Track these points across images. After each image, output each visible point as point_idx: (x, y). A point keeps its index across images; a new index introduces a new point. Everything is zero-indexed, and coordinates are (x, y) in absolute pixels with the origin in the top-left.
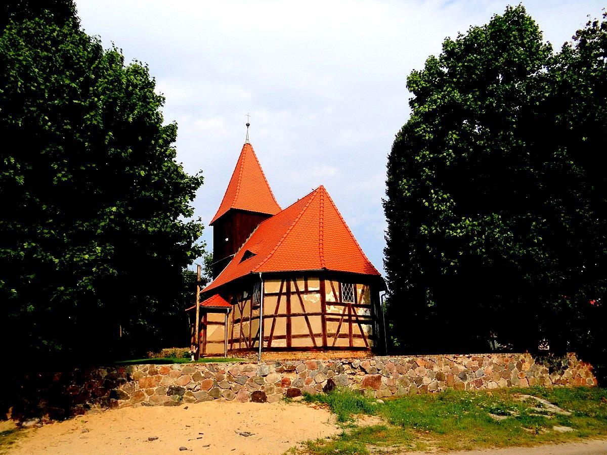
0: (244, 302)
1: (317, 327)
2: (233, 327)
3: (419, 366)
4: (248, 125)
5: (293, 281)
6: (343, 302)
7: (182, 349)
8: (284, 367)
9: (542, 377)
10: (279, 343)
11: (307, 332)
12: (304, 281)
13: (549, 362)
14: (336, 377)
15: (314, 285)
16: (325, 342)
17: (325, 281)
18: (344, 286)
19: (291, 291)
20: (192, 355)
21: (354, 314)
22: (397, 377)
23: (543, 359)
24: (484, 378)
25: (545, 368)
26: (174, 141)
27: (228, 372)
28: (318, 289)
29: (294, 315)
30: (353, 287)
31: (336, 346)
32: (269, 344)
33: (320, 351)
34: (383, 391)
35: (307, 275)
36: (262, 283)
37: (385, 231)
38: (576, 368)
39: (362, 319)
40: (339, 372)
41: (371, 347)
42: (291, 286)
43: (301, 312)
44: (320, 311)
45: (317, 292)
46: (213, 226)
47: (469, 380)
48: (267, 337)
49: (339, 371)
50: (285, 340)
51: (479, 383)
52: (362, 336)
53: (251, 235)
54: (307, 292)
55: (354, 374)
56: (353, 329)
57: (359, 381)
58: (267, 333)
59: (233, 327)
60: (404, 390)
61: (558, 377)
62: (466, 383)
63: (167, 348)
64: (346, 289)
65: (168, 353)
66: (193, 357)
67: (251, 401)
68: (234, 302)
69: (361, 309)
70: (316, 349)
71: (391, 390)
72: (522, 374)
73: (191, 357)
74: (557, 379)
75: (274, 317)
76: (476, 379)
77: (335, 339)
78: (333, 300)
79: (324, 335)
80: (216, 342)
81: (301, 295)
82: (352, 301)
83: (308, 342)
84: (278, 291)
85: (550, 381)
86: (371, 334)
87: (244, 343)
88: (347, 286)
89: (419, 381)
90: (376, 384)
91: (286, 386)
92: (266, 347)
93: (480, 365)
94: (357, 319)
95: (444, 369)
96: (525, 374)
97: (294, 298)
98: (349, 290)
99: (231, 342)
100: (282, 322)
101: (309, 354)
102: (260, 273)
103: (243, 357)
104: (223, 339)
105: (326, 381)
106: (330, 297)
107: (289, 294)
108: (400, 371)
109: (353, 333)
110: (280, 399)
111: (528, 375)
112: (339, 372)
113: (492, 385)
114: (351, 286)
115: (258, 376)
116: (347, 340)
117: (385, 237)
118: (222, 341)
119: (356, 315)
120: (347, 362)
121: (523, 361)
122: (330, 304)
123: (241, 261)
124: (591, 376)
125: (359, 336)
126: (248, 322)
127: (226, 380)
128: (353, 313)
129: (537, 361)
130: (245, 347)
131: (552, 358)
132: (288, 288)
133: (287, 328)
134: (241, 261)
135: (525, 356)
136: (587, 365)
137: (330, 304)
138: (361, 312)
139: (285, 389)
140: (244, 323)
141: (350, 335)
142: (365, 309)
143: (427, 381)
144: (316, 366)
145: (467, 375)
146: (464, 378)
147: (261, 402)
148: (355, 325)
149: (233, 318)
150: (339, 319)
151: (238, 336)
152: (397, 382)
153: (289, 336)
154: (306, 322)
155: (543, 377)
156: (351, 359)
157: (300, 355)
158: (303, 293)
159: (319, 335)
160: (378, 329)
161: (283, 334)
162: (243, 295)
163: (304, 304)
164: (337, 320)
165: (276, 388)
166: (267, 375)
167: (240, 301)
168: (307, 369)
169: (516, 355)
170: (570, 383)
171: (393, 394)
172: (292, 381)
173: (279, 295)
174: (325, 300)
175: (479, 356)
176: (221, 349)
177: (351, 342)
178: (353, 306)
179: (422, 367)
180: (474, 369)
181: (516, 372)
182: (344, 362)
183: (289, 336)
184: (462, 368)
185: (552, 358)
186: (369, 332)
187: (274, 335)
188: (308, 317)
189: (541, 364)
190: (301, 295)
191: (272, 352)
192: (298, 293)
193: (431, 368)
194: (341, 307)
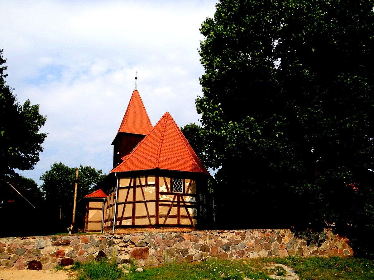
1: (152, 212)
3: (185, 240)
4: (136, 78)
6: (173, 192)
8: (60, 241)
9: (300, 249)
10: (127, 222)
11: (145, 214)
12: (155, 177)
13: (307, 235)
14: (107, 249)
15: (152, 180)
16: (157, 221)
17: (160, 177)
19: (137, 185)
20: (70, 231)
21: (182, 201)
22: (163, 249)
23: (301, 234)
24: (246, 250)
25: (303, 241)
26: (3, 67)
27: (9, 245)
28: (154, 183)
29: (138, 202)
30: (182, 181)
31: (166, 224)
32: (121, 223)
34: (151, 260)
35: (147, 173)
36: (118, 180)
38: (333, 241)
40: (110, 245)
43: (142, 199)
44: (154, 198)
45: (153, 185)
47: (232, 251)
48: (119, 218)
49: (110, 244)
50: (131, 220)
51: (241, 253)
52: (188, 217)
54: (147, 185)
55: (126, 247)
57: (129, 252)
58: (120, 215)
60: (169, 260)
61: (315, 248)
62: (229, 253)
64: (176, 183)
66: (70, 232)
67: (27, 269)
69: (188, 197)
70: (151, 226)
71: (158, 260)
72: (282, 246)
73: (69, 233)
74: (314, 250)
76: (238, 250)
78: (165, 191)
79: (157, 216)
80: (95, 222)
81: (143, 188)
82: (181, 192)
83: (145, 222)
84: (128, 186)
85: (308, 252)
86: (196, 215)
88: (178, 180)
89: (185, 252)
90: (144, 254)
91: (60, 256)
92: (118, 225)
93: (243, 239)
94: (185, 204)
95: (208, 242)
96: (285, 246)
97: (138, 190)
98: (179, 183)
100: (129, 207)
101: (147, 230)
102: (116, 173)
105: (98, 253)
106: (163, 189)
107: (135, 187)
108: (168, 244)
109: (181, 215)
110: (54, 268)
111: (287, 246)
112: (110, 245)
113: (253, 255)
114: (181, 181)
115: (35, 248)
116: (147, 219)
118: (100, 221)
119: (184, 202)
120: (119, 237)
121: (283, 235)
122: (163, 193)
124: (347, 247)
125: (185, 217)
127: (6, 252)
128: (181, 200)
129: (296, 236)
131: (310, 233)
133: (132, 212)
135: (285, 232)
136: (344, 238)
137: (163, 193)
138: (188, 199)
139: (59, 259)
141: (178, 216)
142: (191, 197)
143: (192, 252)
144: (89, 241)
145: (230, 247)
146: (227, 249)
147: (36, 269)
150: (170, 204)
152: (164, 253)
153: (133, 217)
154: (145, 207)
155: (301, 248)
156: (122, 235)
157: (140, 230)
158: (144, 186)
159: (153, 216)
161: (130, 216)
165: (51, 258)
166: (44, 248)
168: (81, 243)
169: (277, 230)
170: (327, 253)
171: (160, 263)
172: (66, 252)
173: (128, 188)
174: (159, 191)
175: (242, 232)
176: (99, 226)
177: (178, 221)
178: (182, 195)
179: (188, 241)
180: (237, 242)
181: (276, 245)
182: (117, 237)
183: (133, 217)
184: (226, 241)
185: (310, 233)
186: (194, 213)
187: (124, 216)
188: (147, 203)
189: (300, 238)
190: (143, 188)
192: (141, 186)
193: (197, 241)
194: (172, 196)
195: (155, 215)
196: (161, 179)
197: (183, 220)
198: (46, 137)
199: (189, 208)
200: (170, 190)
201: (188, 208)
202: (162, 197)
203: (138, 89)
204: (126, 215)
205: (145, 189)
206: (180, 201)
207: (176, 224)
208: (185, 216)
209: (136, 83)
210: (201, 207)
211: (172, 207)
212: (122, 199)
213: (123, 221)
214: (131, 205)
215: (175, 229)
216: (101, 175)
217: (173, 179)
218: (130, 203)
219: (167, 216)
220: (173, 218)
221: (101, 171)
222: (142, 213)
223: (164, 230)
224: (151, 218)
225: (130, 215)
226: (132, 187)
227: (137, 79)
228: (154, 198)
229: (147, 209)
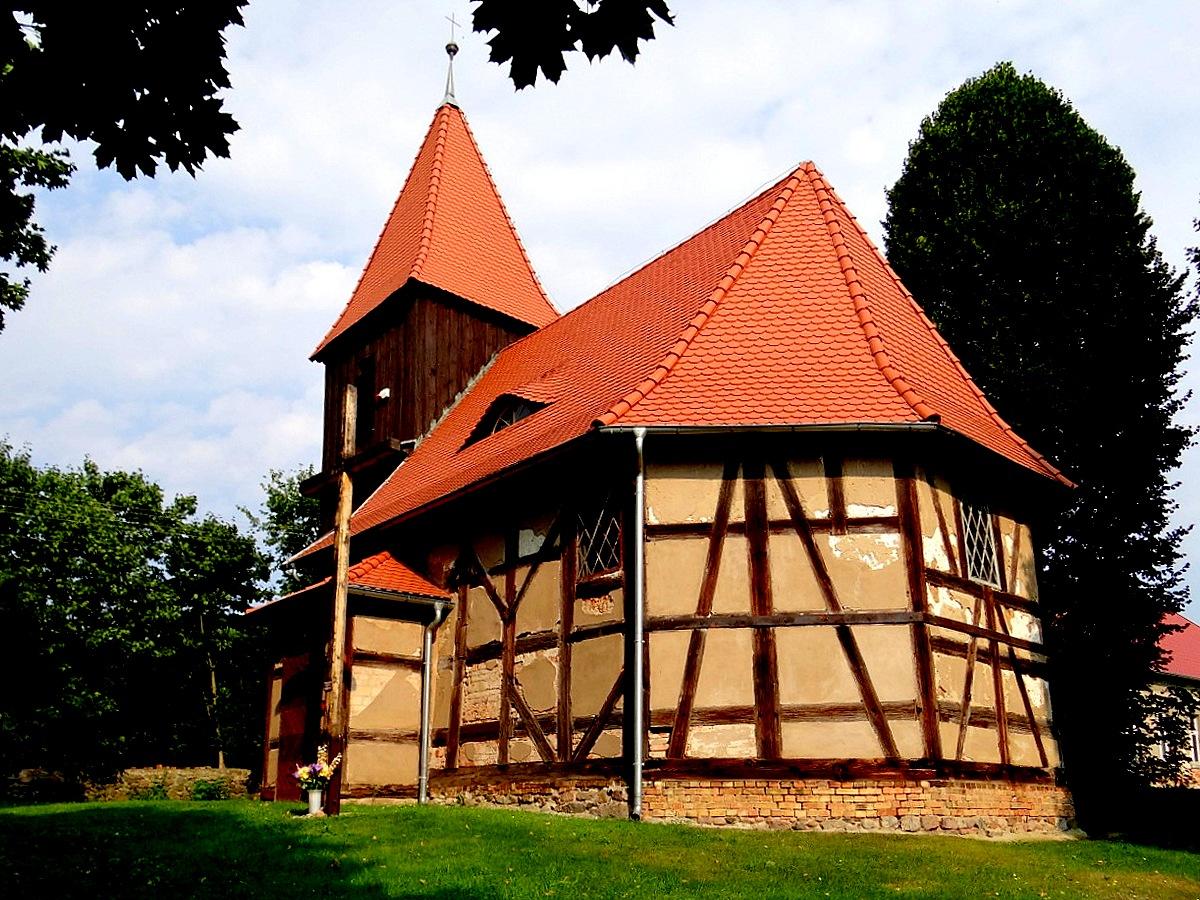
0: (521, 574)
1: (894, 679)
2: (459, 680)
4: (452, 50)
5: (777, 476)
7: (187, 772)
16: (932, 740)
18: (967, 515)
20: (312, 787)
28: (891, 511)
29: (789, 620)
30: (989, 523)
32: (678, 744)
33: (917, 779)
43: (819, 605)
44: (902, 602)
46: (322, 366)
48: (666, 715)
50: (752, 727)
53: (471, 383)
54: (839, 522)
58: (665, 695)
59: (459, 680)
63: (140, 766)
65: (142, 783)
66: (315, 797)
68: (466, 578)
70: (893, 768)
73: (305, 798)
81: (818, 538)
82: (994, 581)
83: (857, 741)
84: (708, 516)
87: (529, 742)
92: (662, 755)
97: (784, 550)
99: (452, 736)
101: (869, 791)
102: (640, 432)
103: (521, 802)
104: (411, 724)
107: (757, 528)
123: (469, 443)
126: (552, 653)
130: (535, 757)
132: (756, 504)
134: (469, 443)
140: (527, 659)
149: (459, 639)
151: (492, 712)
158: (823, 525)
159: (904, 710)
162: (513, 546)
167: (495, 572)
173: (715, 531)
183: (767, 712)
190: (818, 538)
191: (693, 783)
192: (801, 525)
198: (66, 182)
201: (1023, 676)
205: (832, 544)
214: (744, 637)
216: (189, 520)
221: (193, 500)
222: (825, 684)
223: (964, 792)
227: (455, 53)
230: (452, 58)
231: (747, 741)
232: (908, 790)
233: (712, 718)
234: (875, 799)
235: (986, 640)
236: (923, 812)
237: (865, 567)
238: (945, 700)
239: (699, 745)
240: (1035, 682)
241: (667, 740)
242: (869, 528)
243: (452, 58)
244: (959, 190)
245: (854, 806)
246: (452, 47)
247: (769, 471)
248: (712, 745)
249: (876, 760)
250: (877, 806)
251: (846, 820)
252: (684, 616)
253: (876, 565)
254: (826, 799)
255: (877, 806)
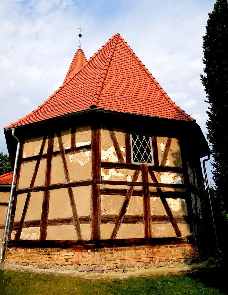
4: (80, 36)
6: (132, 162)
16: (96, 232)
28: (89, 143)
31: (119, 237)
32: (18, 235)
33: (87, 248)
36: (19, 144)
37: (205, 101)
39: (171, 190)
41: (188, 237)
42: (54, 144)
45: (87, 148)
48: (17, 224)
50: (39, 228)
54: (74, 149)
56: (152, 207)
64: (138, 144)
75: (28, 191)
77: (117, 225)
78: (115, 159)
81: (66, 156)
88: (141, 138)
94: (159, 190)
97: (57, 161)
98: (145, 144)
101: (70, 253)
107: (50, 155)
109: (152, 214)
114: (148, 139)
116: (72, 227)
117: (206, 112)
119: (156, 184)
122: (108, 165)
125: (162, 219)
128: (150, 180)
132: (51, 147)
137: (108, 165)
148: (155, 201)
150: (125, 190)
157: (56, 254)
158: (68, 151)
159: (85, 220)
160: (199, 205)
163: (68, 168)
164: (122, 192)
173: (37, 158)
177: (147, 230)
178: (151, 169)
195: (92, 217)
196: (105, 134)
197: (157, 227)
199: (168, 197)
200: (124, 158)
201: (167, 199)
202: (107, 174)
203: (82, 48)
204: (29, 218)
205: (70, 157)
206: (149, 182)
207: (142, 236)
208: (161, 217)
209: (80, 41)
210: (192, 195)
211: (132, 197)
212: (24, 183)
213: (23, 229)
215: (140, 249)
217: (131, 135)
218: (38, 189)
219: (120, 219)
220: (135, 222)
222: (62, 211)
224: (81, 223)
225: (38, 217)
226: (45, 156)
228: (89, 176)
229: (73, 204)
230: (80, 38)
231: (37, 233)
232: (83, 253)
233: (29, 225)
234: (72, 257)
235: (141, 187)
236: (87, 263)
237: (79, 165)
238: (106, 214)
239: (24, 235)
240: (176, 200)
241: (16, 233)
242: (81, 150)
243: (80, 38)
244: (217, 30)
245: (64, 260)
246: (80, 35)
247: (55, 135)
248: (27, 235)
249: (75, 240)
250: (72, 260)
251: (61, 266)
252: (27, 188)
253: (82, 163)
254: (56, 257)
255: (72, 260)
